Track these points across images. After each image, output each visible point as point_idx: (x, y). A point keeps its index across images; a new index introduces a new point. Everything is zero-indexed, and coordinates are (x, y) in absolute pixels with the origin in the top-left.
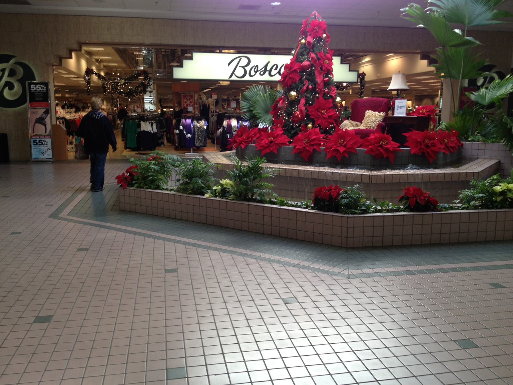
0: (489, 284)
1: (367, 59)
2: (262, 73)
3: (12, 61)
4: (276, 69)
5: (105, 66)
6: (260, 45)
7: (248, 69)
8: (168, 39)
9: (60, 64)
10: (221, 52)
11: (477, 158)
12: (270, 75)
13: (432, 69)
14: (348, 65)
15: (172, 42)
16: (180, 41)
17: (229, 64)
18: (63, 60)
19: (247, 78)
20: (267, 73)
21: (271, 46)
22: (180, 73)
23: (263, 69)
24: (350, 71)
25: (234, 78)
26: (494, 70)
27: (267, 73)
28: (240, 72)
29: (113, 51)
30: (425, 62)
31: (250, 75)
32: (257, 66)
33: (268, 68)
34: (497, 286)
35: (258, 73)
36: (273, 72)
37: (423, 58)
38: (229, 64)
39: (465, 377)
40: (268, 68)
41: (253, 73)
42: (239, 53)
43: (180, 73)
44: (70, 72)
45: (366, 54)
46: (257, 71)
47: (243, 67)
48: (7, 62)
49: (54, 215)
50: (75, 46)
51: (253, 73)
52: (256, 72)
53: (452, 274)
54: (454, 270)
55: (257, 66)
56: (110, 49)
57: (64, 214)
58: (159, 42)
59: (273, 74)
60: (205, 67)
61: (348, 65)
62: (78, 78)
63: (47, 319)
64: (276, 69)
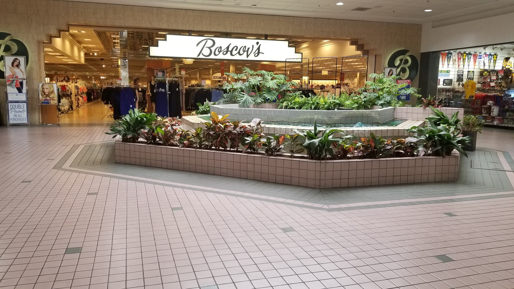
0: (445, 213)
1: (305, 45)
2: (225, 53)
3: (7, 38)
4: (236, 50)
5: (84, 47)
6: (223, 30)
7: (213, 49)
8: (145, 23)
9: (50, 42)
10: (190, 35)
11: (407, 120)
12: (232, 55)
13: (359, 53)
14: (294, 48)
15: (149, 26)
16: (156, 25)
17: (197, 45)
18: (53, 39)
19: (212, 56)
20: (229, 53)
21: (232, 32)
22: (154, 51)
23: (226, 50)
24: (296, 53)
25: (201, 56)
26: (407, 54)
27: (229, 53)
28: (206, 52)
29: (94, 34)
30: (354, 47)
31: (215, 55)
32: (221, 47)
33: (230, 49)
34: (450, 215)
35: (222, 53)
36: (234, 52)
37: (352, 44)
38: (197, 45)
39: (399, 283)
40: (230, 49)
41: (217, 53)
42: (203, 36)
43: (154, 51)
44: (56, 50)
45: (305, 40)
46: (221, 51)
47: (209, 48)
48: (3, 39)
49: (58, 167)
50: (64, 27)
51: (217, 53)
52: (220, 52)
53: (420, 206)
54: (412, 204)
55: (221, 47)
56: (91, 31)
57: (67, 165)
58: (138, 26)
59: (233, 54)
60: (175, 47)
61: (294, 48)
62: (62, 56)
63: (78, 250)
64: (236, 50)
